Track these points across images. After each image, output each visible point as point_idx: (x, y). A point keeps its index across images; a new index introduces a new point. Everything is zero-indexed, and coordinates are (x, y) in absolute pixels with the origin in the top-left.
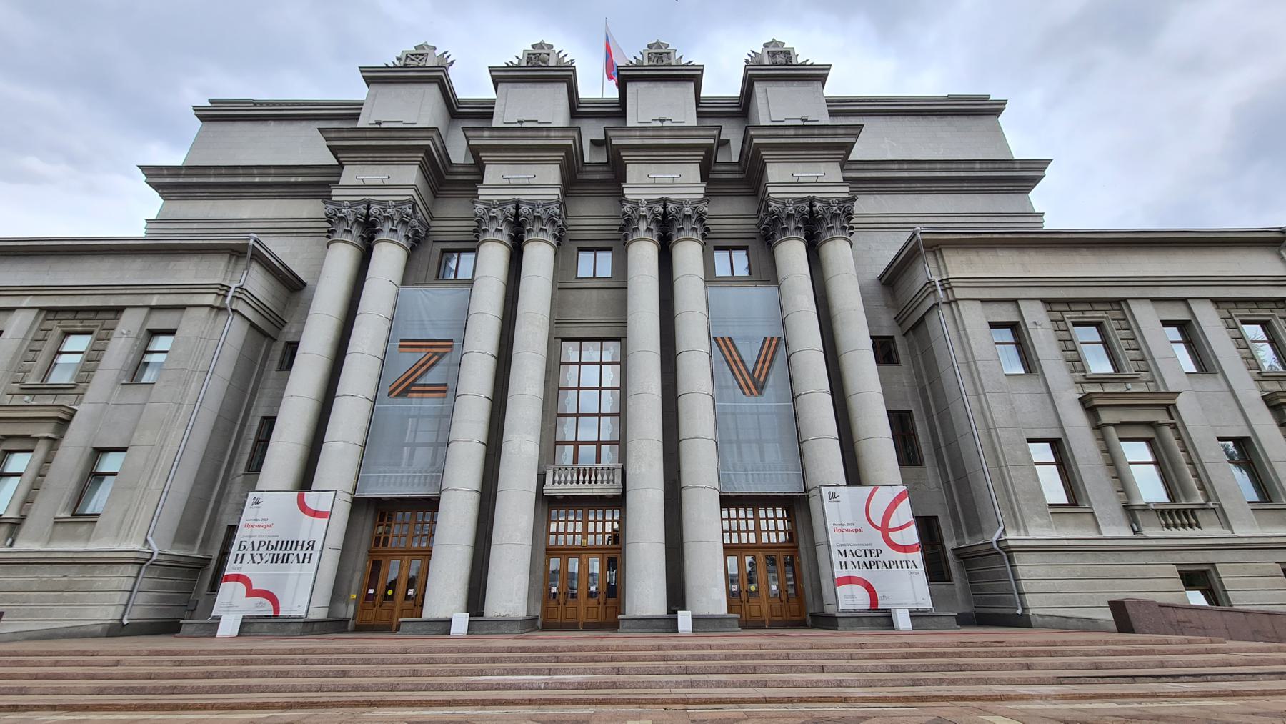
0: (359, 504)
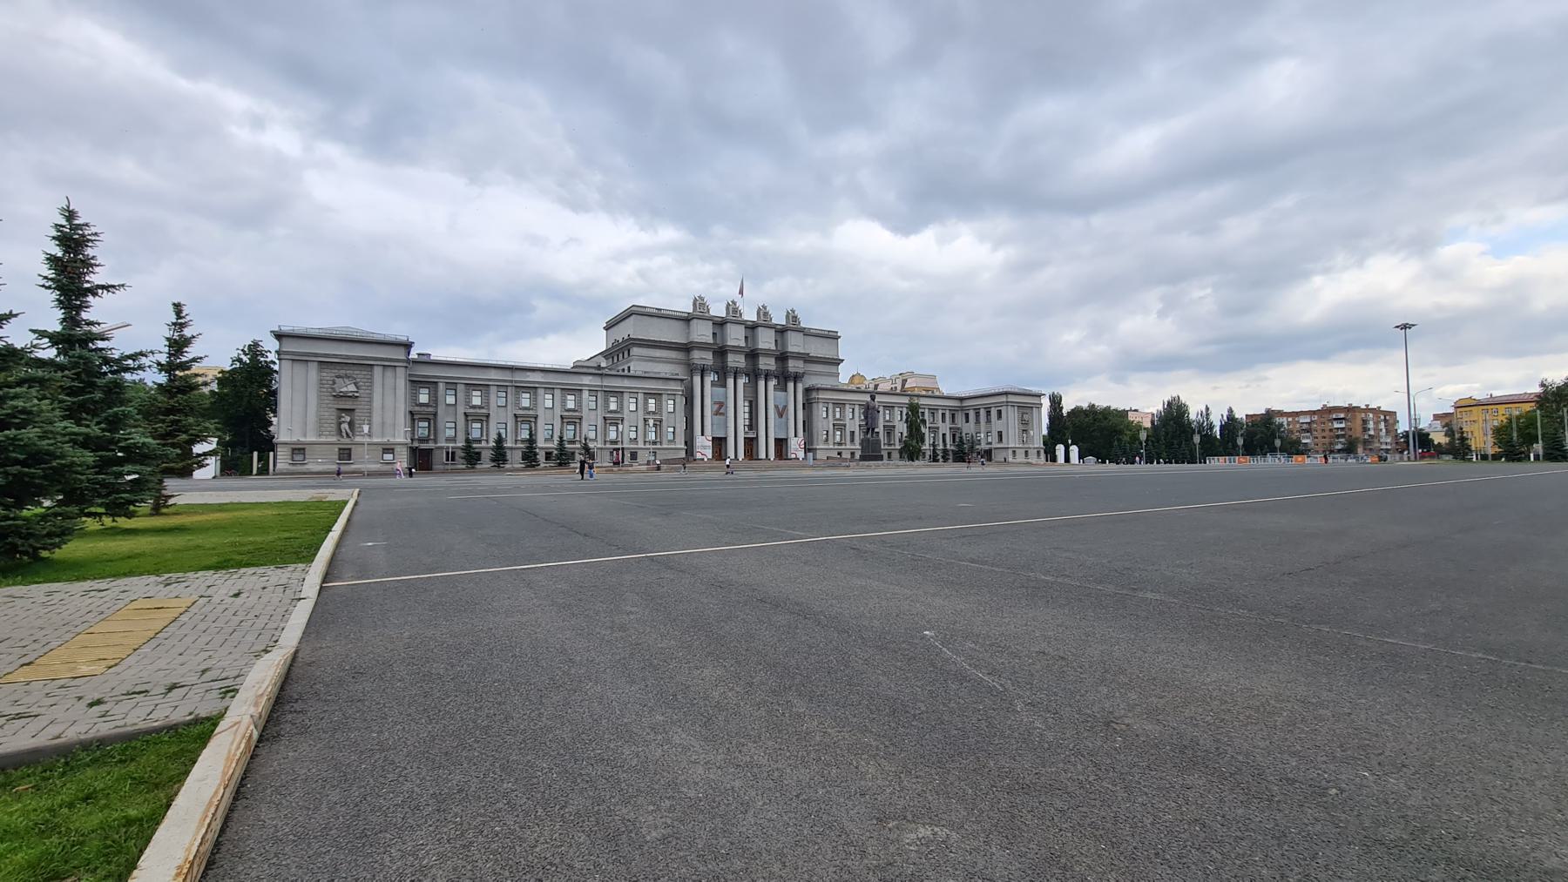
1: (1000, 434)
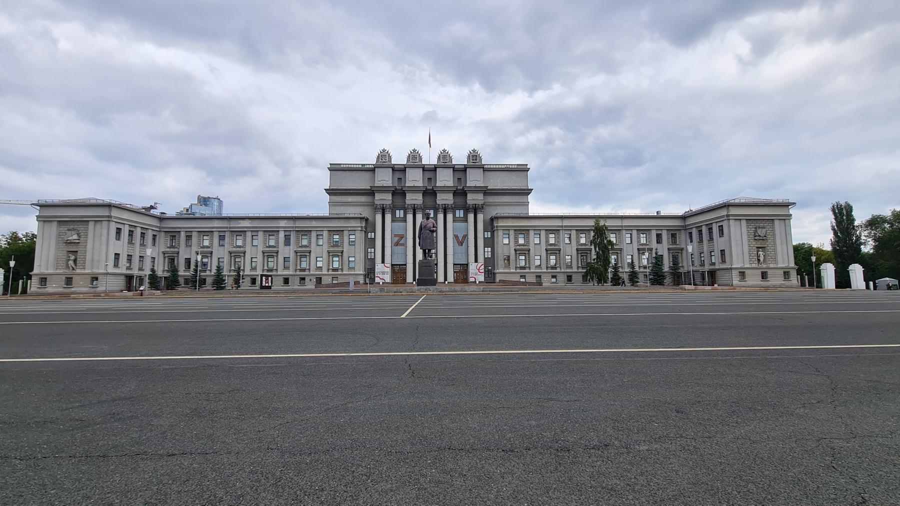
0: (392, 265)
1: (723, 252)
